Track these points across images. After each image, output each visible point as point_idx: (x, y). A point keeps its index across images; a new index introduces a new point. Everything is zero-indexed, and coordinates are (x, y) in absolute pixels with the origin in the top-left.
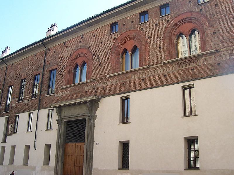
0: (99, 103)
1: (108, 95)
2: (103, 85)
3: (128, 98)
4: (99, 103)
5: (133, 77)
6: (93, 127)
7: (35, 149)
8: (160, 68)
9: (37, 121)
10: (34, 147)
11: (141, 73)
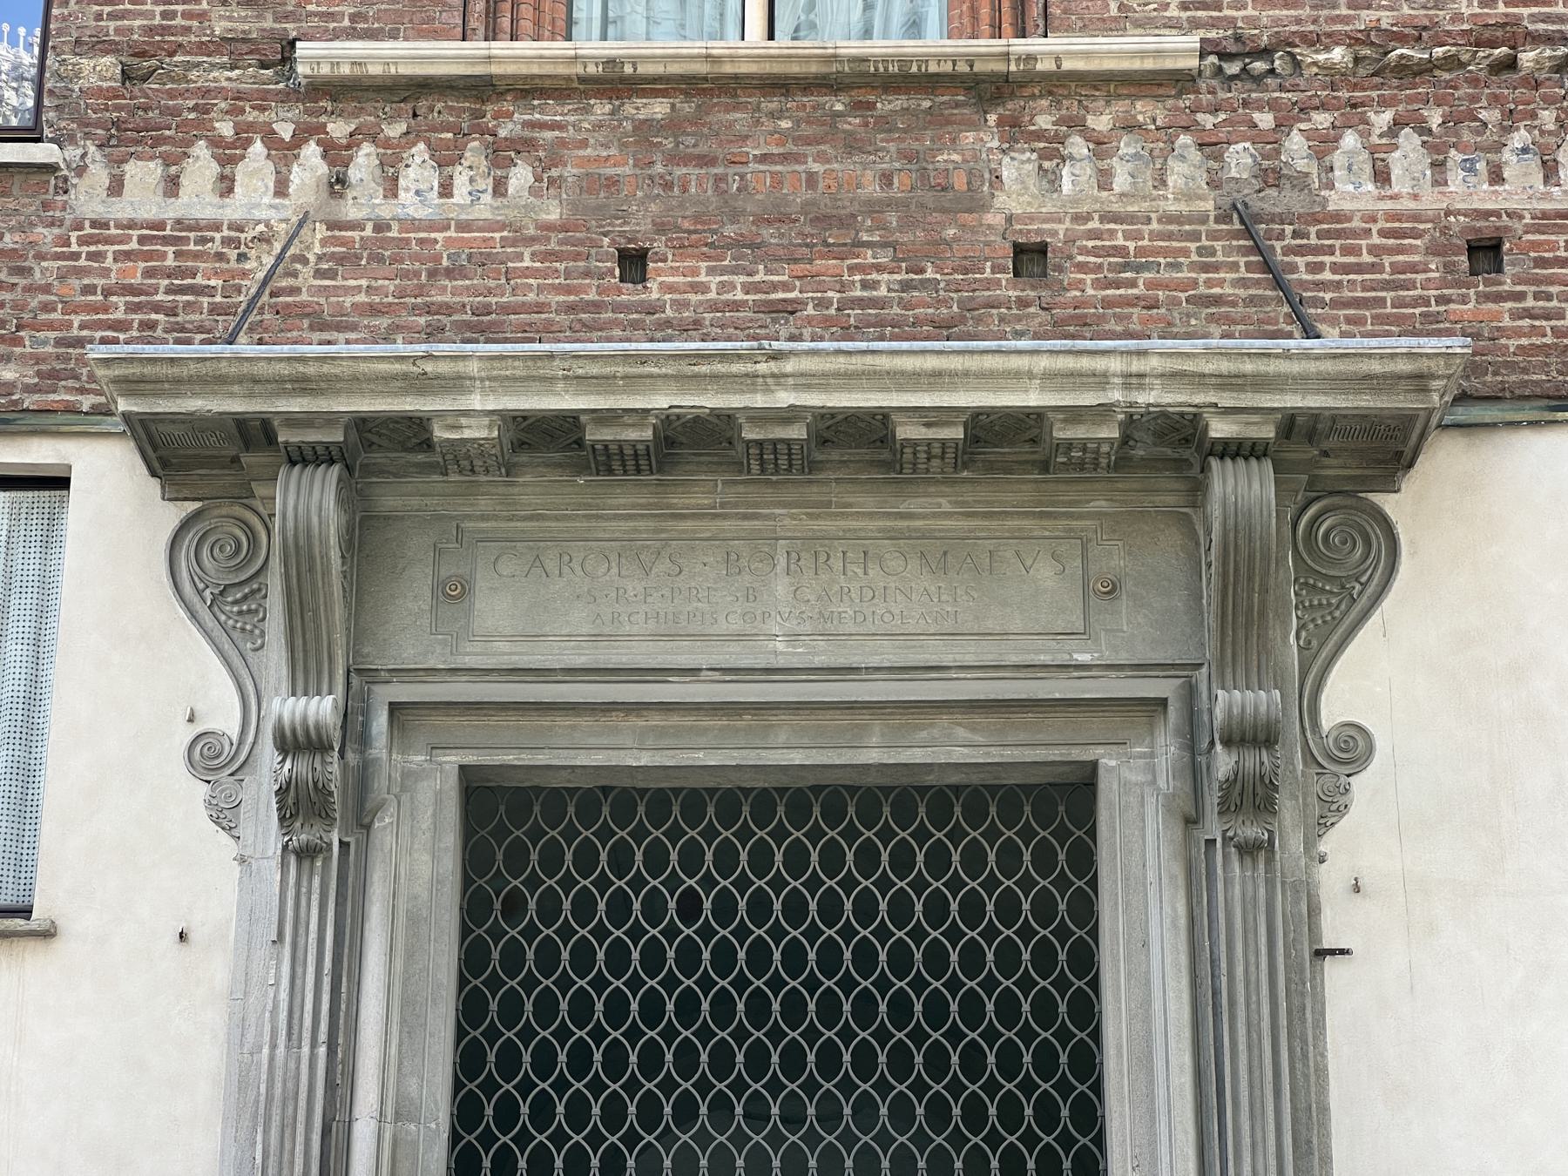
0: (1388, 503)
2: (1467, 192)
4: (1388, 503)
6: (1294, 968)
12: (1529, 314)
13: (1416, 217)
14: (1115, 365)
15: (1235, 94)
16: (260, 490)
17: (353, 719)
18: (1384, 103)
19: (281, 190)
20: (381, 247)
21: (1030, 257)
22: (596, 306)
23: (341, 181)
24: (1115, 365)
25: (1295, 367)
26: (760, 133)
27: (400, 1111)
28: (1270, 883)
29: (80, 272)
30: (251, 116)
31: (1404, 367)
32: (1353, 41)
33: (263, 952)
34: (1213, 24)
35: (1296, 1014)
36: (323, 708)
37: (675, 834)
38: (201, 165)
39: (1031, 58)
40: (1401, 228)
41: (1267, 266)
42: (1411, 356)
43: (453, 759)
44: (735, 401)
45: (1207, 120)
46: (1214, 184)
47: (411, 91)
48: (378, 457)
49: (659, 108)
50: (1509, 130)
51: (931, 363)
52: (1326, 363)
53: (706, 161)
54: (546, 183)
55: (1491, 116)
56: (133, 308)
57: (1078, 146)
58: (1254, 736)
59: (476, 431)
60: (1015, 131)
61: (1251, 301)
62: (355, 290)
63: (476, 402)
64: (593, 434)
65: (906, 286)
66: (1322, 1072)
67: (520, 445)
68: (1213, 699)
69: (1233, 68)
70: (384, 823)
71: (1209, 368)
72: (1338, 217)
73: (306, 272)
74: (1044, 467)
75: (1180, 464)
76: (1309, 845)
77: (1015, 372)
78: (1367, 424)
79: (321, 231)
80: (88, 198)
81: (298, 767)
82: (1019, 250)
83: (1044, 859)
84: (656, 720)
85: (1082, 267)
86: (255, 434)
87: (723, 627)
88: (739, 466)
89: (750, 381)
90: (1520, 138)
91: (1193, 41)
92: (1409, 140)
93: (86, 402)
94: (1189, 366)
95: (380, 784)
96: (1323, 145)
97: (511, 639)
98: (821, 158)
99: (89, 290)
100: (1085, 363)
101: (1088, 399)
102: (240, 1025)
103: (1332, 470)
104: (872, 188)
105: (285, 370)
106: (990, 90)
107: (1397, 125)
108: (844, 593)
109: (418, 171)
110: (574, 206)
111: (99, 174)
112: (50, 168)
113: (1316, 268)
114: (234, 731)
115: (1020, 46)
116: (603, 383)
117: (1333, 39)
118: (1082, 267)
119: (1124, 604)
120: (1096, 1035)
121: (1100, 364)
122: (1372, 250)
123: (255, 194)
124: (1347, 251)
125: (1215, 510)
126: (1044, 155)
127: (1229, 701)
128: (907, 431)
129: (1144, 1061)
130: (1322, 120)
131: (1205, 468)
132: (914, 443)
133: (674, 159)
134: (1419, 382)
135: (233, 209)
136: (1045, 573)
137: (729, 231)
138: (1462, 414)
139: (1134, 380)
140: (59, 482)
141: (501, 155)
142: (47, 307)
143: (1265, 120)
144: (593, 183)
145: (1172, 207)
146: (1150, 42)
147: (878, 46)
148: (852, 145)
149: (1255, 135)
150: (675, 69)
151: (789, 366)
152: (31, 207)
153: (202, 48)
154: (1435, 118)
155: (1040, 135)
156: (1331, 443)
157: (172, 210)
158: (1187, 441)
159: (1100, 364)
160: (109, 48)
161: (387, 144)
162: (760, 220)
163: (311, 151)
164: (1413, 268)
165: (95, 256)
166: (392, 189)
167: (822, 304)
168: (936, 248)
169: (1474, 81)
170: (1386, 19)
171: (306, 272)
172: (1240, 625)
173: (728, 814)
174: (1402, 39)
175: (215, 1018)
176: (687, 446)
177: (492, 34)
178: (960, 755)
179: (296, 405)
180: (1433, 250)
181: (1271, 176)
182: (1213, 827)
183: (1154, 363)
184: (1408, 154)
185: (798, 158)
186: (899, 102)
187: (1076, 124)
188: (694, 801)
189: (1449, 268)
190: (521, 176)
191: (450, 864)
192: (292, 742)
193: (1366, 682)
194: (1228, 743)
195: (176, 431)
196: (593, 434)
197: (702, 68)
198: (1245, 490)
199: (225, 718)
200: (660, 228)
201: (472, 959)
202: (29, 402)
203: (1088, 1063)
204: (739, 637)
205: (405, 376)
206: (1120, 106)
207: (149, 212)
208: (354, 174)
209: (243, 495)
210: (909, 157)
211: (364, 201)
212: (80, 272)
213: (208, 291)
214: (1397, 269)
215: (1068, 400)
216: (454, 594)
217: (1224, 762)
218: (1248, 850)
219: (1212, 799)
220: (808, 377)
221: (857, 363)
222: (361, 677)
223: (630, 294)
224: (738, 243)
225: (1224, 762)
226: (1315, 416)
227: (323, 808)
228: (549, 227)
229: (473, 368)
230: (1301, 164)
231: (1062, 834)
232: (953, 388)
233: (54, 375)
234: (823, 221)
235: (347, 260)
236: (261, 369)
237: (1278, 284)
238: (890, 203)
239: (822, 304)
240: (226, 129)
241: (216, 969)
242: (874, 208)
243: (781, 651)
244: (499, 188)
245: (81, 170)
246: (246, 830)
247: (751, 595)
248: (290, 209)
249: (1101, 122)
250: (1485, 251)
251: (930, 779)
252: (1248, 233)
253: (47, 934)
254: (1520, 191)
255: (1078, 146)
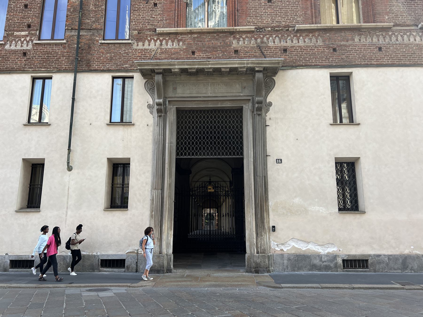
0: (274, 78)
1: (298, 66)
2: (283, 44)
3: (347, 78)
4: (274, 78)
5: (357, 40)
6: (263, 127)
7: (70, 169)
8: (414, 34)
9: (73, 99)
10: (68, 163)
11: (375, 37)
12: (290, 57)
13: (278, 47)
14: (246, 62)
15: (258, 33)
16: (154, 78)
17: (164, 102)
18: (274, 34)
19: (155, 45)
20: (166, 51)
21: (236, 51)
22: (189, 58)
23: (162, 44)
24: (246, 62)
25: (265, 62)
26: (207, 38)
27: (171, 143)
28: (261, 119)
29: (134, 55)
30: (152, 37)
31: (277, 61)
32: (271, 27)
33: (156, 127)
34: (256, 26)
35: (264, 132)
36: (161, 101)
37: (199, 115)
38: (147, 43)
39: (236, 29)
40: (276, 48)
41: (262, 52)
42: (278, 60)
43: (175, 107)
44: (204, 67)
45: (255, 36)
46: (256, 43)
47: (169, 34)
48: (166, 74)
49: (196, 36)
50: (288, 37)
51: (226, 62)
52: (267, 61)
53: (201, 41)
54: (184, 44)
55: (286, 35)
56: (140, 58)
57: (241, 39)
58: (260, 102)
59: (176, 70)
60: (235, 38)
61: (260, 56)
62: (163, 56)
63: (176, 67)
64: (189, 71)
65: (223, 55)
66: (266, 138)
67: (181, 72)
68: (255, 99)
69: (258, 30)
70: (168, 113)
71: (256, 62)
72: (270, 47)
73: (158, 54)
74: (238, 74)
75: (252, 74)
76: (265, 114)
77: (235, 63)
78: (272, 68)
79: (160, 50)
80: (135, 47)
81: (159, 107)
82: (235, 51)
83: (237, 117)
84: (197, 102)
85: (242, 53)
86: (153, 71)
87: (203, 92)
88: (205, 75)
89: (206, 64)
90: (289, 38)
91: (254, 27)
92: (277, 38)
93: (135, 69)
94: (254, 62)
95: (167, 109)
96: (268, 39)
97: (181, 94)
98: (214, 41)
99: (135, 56)
100: (242, 62)
101: (243, 66)
102: (154, 134)
103: (269, 74)
104: (219, 44)
105: (156, 63)
106: (232, 33)
107: (276, 36)
108: (216, 88)
109: (170, 43)
110: (187, 47)
111: (136, 44)
112: (131, 43)
113: (267, 52)
114: (152, 104)
115: (235, 28)
116: (190, 65)
117: (269, 27)
118: (242, 53)
119: (246, 89)
120: (242, 135)
121: (244, 62)
122: (273, 50)
123: (152, 46)
124: (270, 50)
125: (256, 78)
126: (238, 40)
127: (257, 99)
128: (223, 70)
129: (248, 137)
130: (268, 36)
131: (255, 74)
132: (224, 71)
133: (197, 41)
134: (278, 63)
135: (150, 48)
136: (237, 86)
137: (204, 49)
138: (282, 68)
139: (248, 64)
140: (132, 77)
141: (179, 41)
142: (131, 58)
143: (262, 36)
144: (189, 44)
145: (252, 46)
146: (249, 27)
147: (220, 28)
148: (217, 39)
149: (261, 38)
150: (197, 31)
151: (210, 63)
152: (129, 48)
153: (146, 30)
154: (280, 36)
155: (237, 38)
156: (269, 71)
157: (144, 48)
158: (253, 71)
159: (244, 62)
160: (137, 30)
161: (166, 40)
162: (207, 48)
163: (158, 41)
164: (277, 52)
165: (136, 53)
166: (167, 45)
167: (214, 57)
168: (226, 51)
169: (284, 32)
170: (275, 25)
171: (158, 54)
172: (258, 92)
173: (204, 112)
174: (276, 27)
175: (151, 133)
176: (200, 72)
177: (178, 27)
178: (228, 105)
179: (157, 67)
180: (279, 50)
181: (262, 42)
182: (255, 113)
183: (250, 61)
184: (277, 40)
185: (211, 41)
186: (222, 35)
187: (241, 37)
188: (201, 111)
189: (281, 52)
190: (181, 43)
191: (175, 117)
192: (158, 104)
193: (271, 97)
194: (257, 103)
195: (144, 71)
196: (189, 71)
197: (200, 31)
198: (259, 76)
199: (151, 103)
200: (196, 49)
201: (178, 128)
202: (129, 69)
203: (242, 138)
204: (205, 93)
205: (169, 64)
206: (246, 35)
207: (141, 48)
208: (163, 43)
209: (152, 79)
210: (223, 41)
211: (164, 46)
212: (134, 55)
213: (148, 56)
214: (276, 52)
215: (240, 66)
216: (175, 89)
217: (257, 105)
218: (259, 115)
219: (255, 110)
220: (212, 64)
221: (218, 62)
222: (165, 98)
223: (193, 56)
224: (204, 51)
225: (257, 105)
226: (267, 67)
227: (161, 111)
228: (184, 49)
229: (176, 63)
230: (265, 41)
231: (239, 114)
232: (228, 65)
233: (132, 66)
234: (214, 48)
235: (162, 53)
236: (153, 63)
237: (263, 54)
238: (221, 46)
239: (214, 57)
240: (149, 39)
241: (151, 129)
242: (219, 46)
243: (210, 95)
244: (179, 45)
245: (134, 43)
246: (154, 114)
247: (206, 89)
248: (156, 47)
249: (244, 37)
250: (285, 50)
251: (225, 108)
252: (260, 49)
253: (133, 125)
254: (289, 44)
255: (241, 39)
